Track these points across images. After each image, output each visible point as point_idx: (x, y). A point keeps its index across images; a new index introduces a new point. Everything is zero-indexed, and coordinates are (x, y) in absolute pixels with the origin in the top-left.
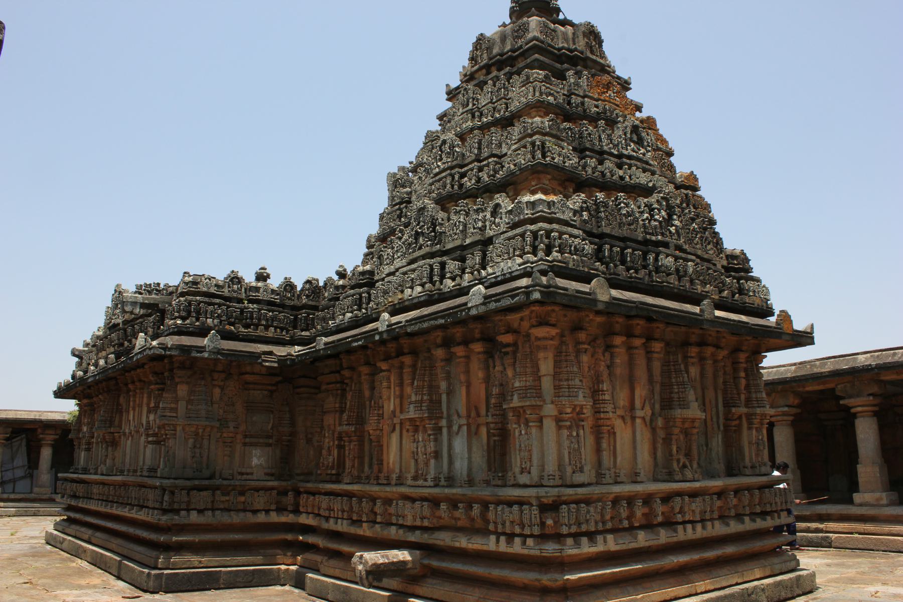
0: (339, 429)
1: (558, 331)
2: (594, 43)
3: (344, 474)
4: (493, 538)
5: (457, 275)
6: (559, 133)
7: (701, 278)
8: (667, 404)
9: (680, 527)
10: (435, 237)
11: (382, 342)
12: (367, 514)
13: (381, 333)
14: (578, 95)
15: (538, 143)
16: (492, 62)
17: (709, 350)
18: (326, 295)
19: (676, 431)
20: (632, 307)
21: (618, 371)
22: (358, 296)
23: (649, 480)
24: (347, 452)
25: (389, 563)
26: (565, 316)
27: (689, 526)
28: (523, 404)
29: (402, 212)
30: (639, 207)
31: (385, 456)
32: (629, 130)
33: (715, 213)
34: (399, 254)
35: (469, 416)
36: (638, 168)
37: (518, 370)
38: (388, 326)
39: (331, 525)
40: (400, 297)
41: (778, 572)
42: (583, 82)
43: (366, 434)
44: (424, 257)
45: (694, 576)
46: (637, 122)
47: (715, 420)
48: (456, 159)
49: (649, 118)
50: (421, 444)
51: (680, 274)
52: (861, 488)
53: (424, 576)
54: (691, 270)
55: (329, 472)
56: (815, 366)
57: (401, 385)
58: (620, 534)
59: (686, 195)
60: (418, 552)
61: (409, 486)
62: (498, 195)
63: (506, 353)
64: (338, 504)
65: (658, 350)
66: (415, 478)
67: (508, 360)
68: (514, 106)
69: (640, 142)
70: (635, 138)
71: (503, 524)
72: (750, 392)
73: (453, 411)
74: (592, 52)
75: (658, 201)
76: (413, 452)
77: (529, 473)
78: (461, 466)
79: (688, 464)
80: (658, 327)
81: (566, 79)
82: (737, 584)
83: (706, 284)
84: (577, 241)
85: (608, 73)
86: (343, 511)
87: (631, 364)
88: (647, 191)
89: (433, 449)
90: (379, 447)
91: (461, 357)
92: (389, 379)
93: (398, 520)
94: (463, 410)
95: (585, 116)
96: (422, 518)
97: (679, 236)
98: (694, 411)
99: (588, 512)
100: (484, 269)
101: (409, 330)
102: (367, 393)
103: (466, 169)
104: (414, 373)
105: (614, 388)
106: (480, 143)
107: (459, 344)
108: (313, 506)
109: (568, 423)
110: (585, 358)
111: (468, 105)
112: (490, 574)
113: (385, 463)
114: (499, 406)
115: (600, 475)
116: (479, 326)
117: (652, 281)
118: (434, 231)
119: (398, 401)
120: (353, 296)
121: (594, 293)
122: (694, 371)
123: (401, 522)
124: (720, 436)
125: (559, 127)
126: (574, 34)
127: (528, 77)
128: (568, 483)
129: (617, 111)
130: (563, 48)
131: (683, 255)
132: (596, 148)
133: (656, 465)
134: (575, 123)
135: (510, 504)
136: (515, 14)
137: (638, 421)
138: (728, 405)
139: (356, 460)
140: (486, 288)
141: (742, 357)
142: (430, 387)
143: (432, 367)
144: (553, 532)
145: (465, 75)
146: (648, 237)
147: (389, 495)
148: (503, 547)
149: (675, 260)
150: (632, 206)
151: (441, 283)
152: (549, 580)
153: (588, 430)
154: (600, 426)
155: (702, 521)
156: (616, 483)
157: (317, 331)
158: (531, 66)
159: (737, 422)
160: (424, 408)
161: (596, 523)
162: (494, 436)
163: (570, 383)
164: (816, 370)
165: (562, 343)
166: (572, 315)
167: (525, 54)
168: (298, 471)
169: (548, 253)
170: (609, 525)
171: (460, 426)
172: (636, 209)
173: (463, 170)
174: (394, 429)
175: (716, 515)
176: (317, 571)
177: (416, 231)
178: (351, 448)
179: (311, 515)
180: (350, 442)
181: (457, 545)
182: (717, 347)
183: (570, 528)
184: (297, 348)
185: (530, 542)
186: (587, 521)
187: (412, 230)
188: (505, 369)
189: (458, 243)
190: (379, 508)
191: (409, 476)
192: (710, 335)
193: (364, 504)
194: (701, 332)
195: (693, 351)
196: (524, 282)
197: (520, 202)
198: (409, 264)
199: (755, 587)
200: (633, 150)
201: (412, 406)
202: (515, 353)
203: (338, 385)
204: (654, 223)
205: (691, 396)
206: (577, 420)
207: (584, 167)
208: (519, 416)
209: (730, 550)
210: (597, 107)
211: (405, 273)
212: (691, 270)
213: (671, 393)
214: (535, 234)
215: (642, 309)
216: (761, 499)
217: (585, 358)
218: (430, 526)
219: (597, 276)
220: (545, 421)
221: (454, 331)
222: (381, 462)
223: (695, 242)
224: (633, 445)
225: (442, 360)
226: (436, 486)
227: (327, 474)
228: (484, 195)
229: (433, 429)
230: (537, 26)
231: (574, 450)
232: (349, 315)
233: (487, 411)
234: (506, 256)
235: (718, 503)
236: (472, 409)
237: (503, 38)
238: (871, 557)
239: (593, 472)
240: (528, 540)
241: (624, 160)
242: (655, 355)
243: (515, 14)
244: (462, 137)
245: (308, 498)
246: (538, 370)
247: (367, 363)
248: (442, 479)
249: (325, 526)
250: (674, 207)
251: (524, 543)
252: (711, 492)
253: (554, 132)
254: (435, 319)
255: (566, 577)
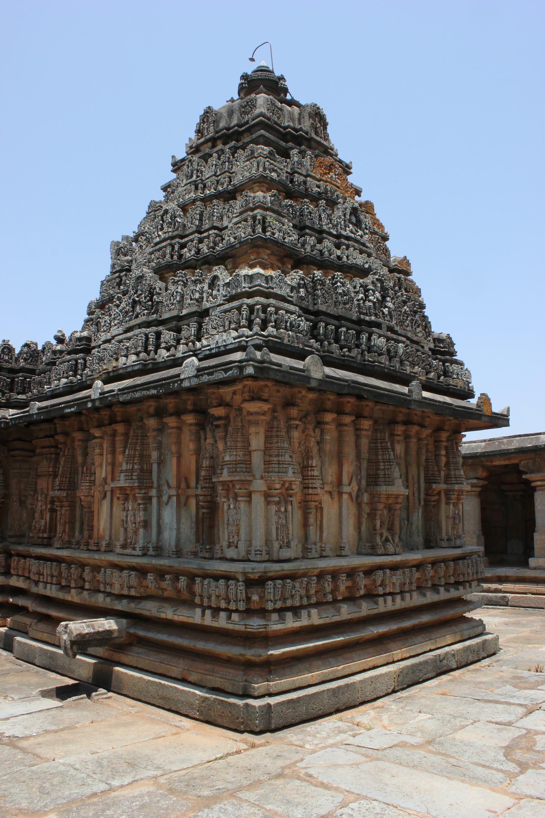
0: (51, 493)
1: (270, 406)
2: (319, 125)
3: (55, 539)
4: (198, 611)
5: (172, 346)
6: (280, 210)
7: (410, 359)
8: (373, 480)
9: (381, 600)
10: (152, 306)
11: (96, 409)
12: (75, 581)
13: (93, 401)
14: (301, 174)
15: (259, 217)
16: (218, 136)
17: (414, 429)
18: (44, 359)
19: (381, 506)
20: (344, 385)
21: (328, 447)
22: (74, 362)
23: (353, 553)
24: (58, 517)
25: (94, 633)
26: (278, 391)
27: (389, 598)
28: (233, 479)
29: (121, 280)
30: (355, 287)
31: (95, 523)
32: (348, 212)
33: (425, 297)
34: (116, 322)
35: (178, 487)
36: (355, 249)
37: (229, 444)
38: (100, 394)
39: (40, 590)
40: (114, 364)
41: (466, 637)
42: (307, 161)
43: (77, 499)
44: (140, 326)
45: (392, 645)
46: (356, 205)
47: (416, 495)
48: (177, 229)
49: (367, 202)
50: (130, 513)
51: (391, 355)
52: (536, 554)
53: (130, 644)
54: (401, 351)
55: (41, 535)
56: (503, 443)
57: (113, 452)
58: (324, 607)
59: (399, 279)
60: (124, 621)
61: (119, 554)
62: (217, 267)
63: (218, 426)
64: (47, 569)
65: (366, 427)
66: (124, 547)
67: (220, 433)
68: (237, 180)
69: (358, 224)
70: (354, 220)
71: (209, 598)
72: (449, 470)
73: (163, 482)
74: (316, 133)
75: (373, 282)
76: (123, 521)
77: (237, 547)
78: (169, 537)
79: (390, 537)
80: (367, 406)
81: (290, 158)
82: (431, 650)
83: (414, 365)
84: (293, 317)
85: (331, 155)
86: (52, 576)
87: (340, 440)
88: (364, 272)
89: (142, 518)
90: (90, 514)
91: (172, 428)
92: (101, 446)
93: (105, 588)
94: (173, 482)
95: (306, 194)
96: (129, 587)
97: (391, 317)
98: (398, 488)
99: (294, 587)
100: (199, 340)
101: (121, 399)
102: (80, 459)
103: (186, 239)
104: (126, 442)
105: (322, 463)
106: (201, 215)
107: (171, 415)
108: (24, 569)
109: (277, 499)
110: (296, 434)
111: (192, 176)
112: (194, 646)
113: (95, 530)
114: (208, 478)
115: (306, 550)
116: (192, 398)
117: (365, 361)
118: (151, 300)
119: (109, 468)
120: (69, 361)
121: (308, 370)
122: (399, 448)
123: (108, 590)
124: (420, 511)
125: (280, 204)
126: (300, 114)
127: (253, 152)
128: (275, 559)
129: (338, 193)
130: (288, 127)
131: (395, 336)
132: (316, 227)
133: (360, 538)
134: (296, 201)
135: (216, 578)
136: (244, 91)
137: (345, 496)
138: (429, 481)
139: (67, 525)
140: (200, 360)
141: (444, 436)
142: (142, 456)
143: (144, 436)
144: (258, 608)
145: (191, 147)
146: (362, 317)
147: (99, 563)
148: (208, 621)
149: (387, 341)
150: (349, 285)
151: (156, 353)
152: (253, 655)
153: (296, 504)
154: (309, 501)
155: (402, 592)
156: (322, 557)
157: (33, 394)
158: (256, 142)
159: (436, 498)
160: (134, 477)
161: (301, 598)
162: (203, 508)
163: (280, 458)
164: (503, 447)
165: (274, 418)
166: (285, 391)
167: (250, 130)
168: (11, 533)
169: (264, 328)
170: (314, 600)
171: (170, 497)
172: (352, 289)
173: (183, 241)
174: (105, 496)
175: (414, 587)
176: (25, 633)
177: (134, 300)
178: (63, 512)
179: (21, 578)
180: (62, 507)
181: (163, 616)
182: (422, 426)
183: (275, 604)
184: (12, 411)
185: (235, 617)
186: (292, 596)
187: (130, 298)
188: (216, 441)
189: (174, 313)
190: (87, 574)
191: (118, 544)
192: (416, 415)
193: (73, 570)
194: (407, 411)
195: (400, 429)
196: (238, 356)
197: (238, 275)
198: (126, 332)
199: (447, 654)
200: (351, 232)
201: (122, 475)
202: (226, 426)
203: (52, 450)
204: (368, 304)
205: (396, 473)
206: (286, 496)
207: (303, 245)
208: (228, 490)
209: (425, 618)
210: (318, 187)
211: (120, 341)
212: (401, 351)
213: (378, 469)
214: (251, 308)
215: (353, 387)
216: (455, 570)
217: (296, 434)
218: (137, 595)
219: (312, 353)
220: (254, 496)
221: (167, 401)
222: (91, 528)
223: (406, 324)
224: (338, 519)
225: (154, 430)
226: (144, 555)
227: (39, 538)
228: (203, 267)
229: (143, 498)
230: (264, 102)
231: (282, 525)
232: (64, 380)
233: (197, 483)
234: (221, 329)
235: (417, 575)
236: (182, 480)
237: (231, 113)
238: (541, 615)
239: (300, 546)
240: (233, 614)
241: (343, 240)
242: (364, 433)
243: (244, 91)
244: (184, 208)
245: (19, 561)
246: (249, 445)
247: (81, 429)
248: (151, 549)
249: (34, 589)
250: (388, 289)
251: (229, 618)
252: (410, 564)
253: (276, 208)
254: (148, 389)
255: (270, 652)
